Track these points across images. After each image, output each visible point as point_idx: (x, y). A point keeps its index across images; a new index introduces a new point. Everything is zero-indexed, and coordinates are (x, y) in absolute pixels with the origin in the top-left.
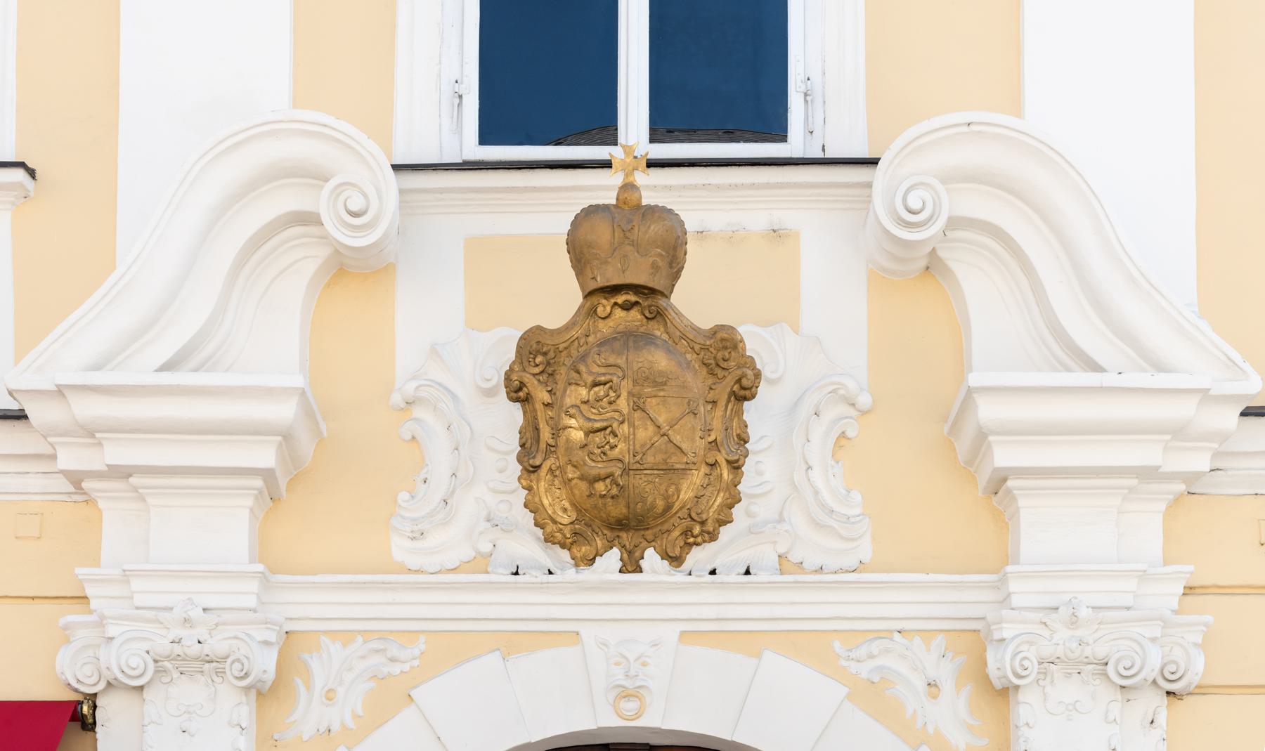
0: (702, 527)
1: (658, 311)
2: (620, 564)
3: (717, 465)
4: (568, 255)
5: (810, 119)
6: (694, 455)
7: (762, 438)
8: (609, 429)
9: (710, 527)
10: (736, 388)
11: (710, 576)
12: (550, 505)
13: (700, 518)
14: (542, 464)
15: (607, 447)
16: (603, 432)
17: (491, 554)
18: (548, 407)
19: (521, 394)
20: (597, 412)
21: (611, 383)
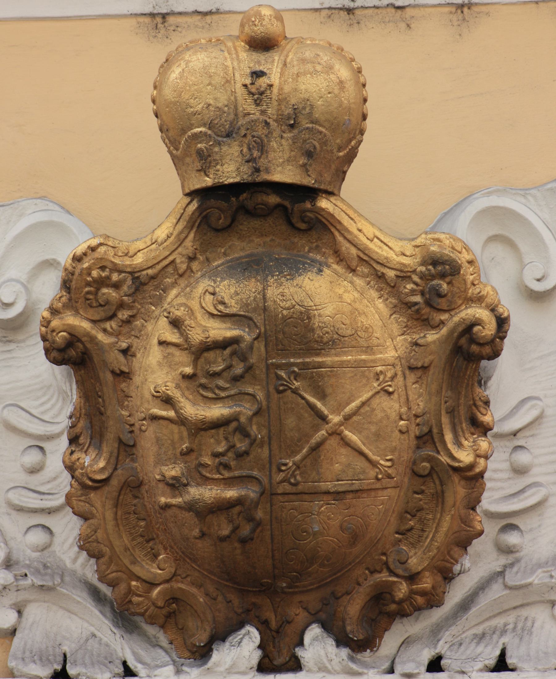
0: (412, 584)
1: (317, 218)
2: (257, 655)
3: (435, 476)
4: (160, 133)
5: (514, 192)
6: (389, 464)
7: (523, 402)
8: (234, 425)
9: (426, 583)
10: (463, 341)
11: (429, 675)
12: (126, 549)
13: (406, 570)
14: (16, 299)
15: (230, 454)
16: (222, 429)
17: (15, 630)
18: (121, 378)
19: (72, 353)
20: (214, 396)
21: (235, 346)
